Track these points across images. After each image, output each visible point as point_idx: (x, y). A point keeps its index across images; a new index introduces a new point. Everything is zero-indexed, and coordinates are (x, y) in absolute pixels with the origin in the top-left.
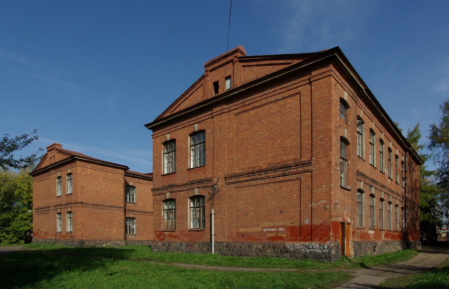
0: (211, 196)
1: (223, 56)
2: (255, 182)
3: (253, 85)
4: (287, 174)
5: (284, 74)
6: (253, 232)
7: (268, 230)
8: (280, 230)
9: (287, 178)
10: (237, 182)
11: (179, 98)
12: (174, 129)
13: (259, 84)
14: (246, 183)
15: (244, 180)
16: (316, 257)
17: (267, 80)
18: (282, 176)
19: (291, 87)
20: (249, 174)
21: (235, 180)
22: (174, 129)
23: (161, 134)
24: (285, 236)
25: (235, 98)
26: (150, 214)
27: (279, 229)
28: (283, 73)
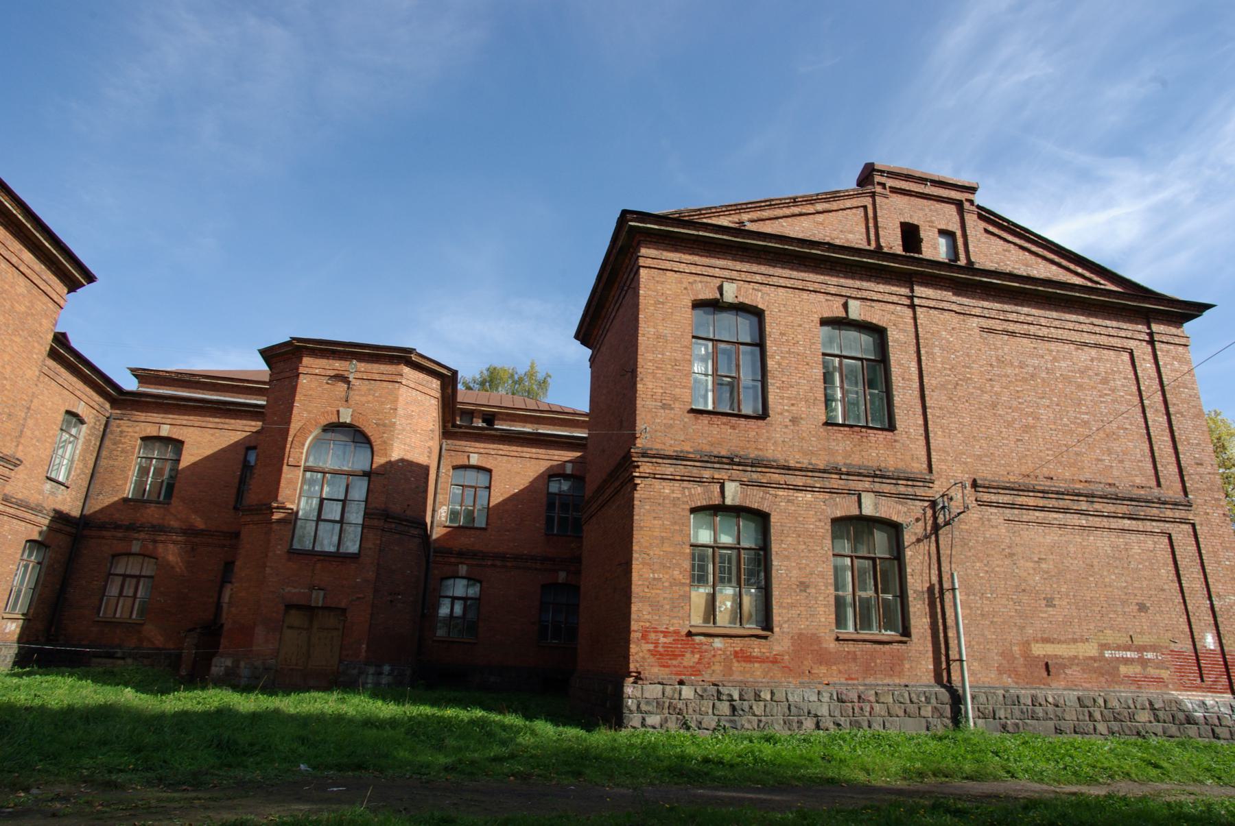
0: (925, 529)
1: (937, 179)
2: (1061, 516)
3: (1041, 286)
4: (1142, 517)
5: (1110, 300)
6: (1076, 657)
7: (1117, 656)
8: (1149, 657)
9: (1139, 525)
10: (1012, 506)
11: (780, 199)
12: (758, 278)
13: (1056, 293)
14: (1037, 514)
15: (1035, 504)
16: (1077, 730)
17: (1073, 294)
18: (1129, 518)
19: (1071, 326)
20: (1048, 493)
21: (1007, 499)
22: (758, 278)
23: (693, 269)
24: (1165, 674)
25: (979, 291)
26: (12, 511)
27: (1145, 653)
28: (1109, 297)
